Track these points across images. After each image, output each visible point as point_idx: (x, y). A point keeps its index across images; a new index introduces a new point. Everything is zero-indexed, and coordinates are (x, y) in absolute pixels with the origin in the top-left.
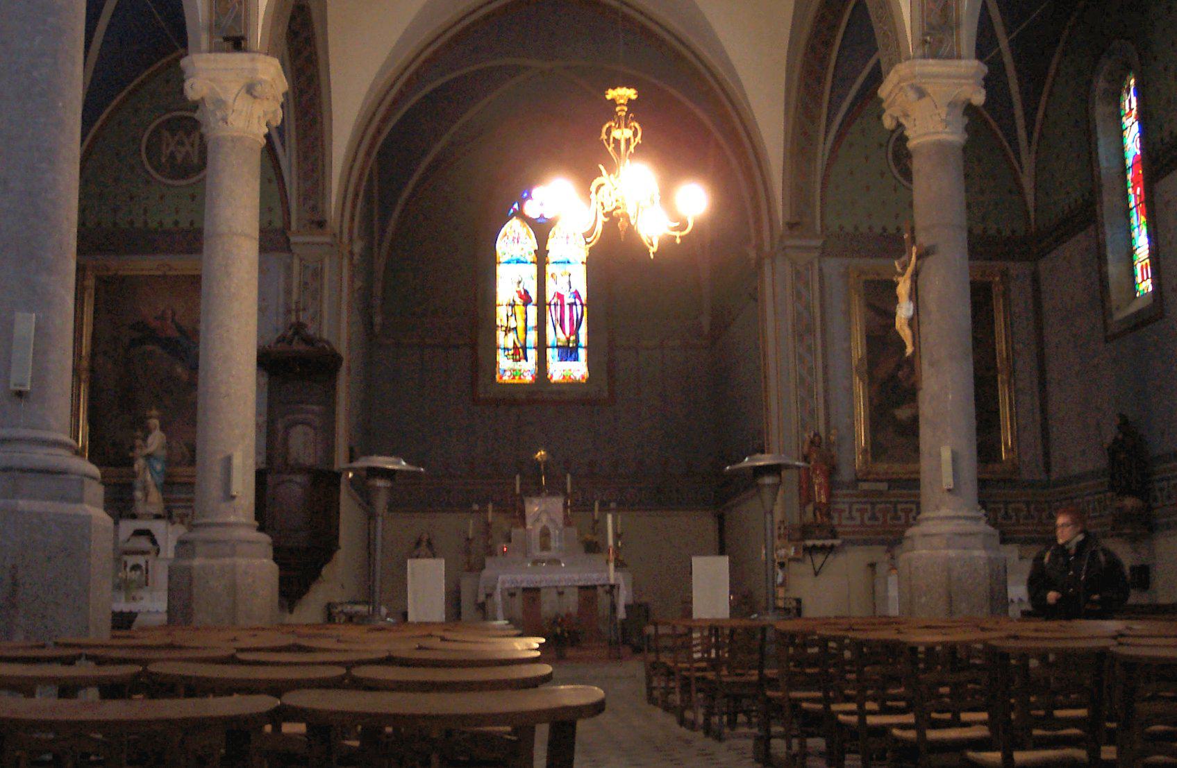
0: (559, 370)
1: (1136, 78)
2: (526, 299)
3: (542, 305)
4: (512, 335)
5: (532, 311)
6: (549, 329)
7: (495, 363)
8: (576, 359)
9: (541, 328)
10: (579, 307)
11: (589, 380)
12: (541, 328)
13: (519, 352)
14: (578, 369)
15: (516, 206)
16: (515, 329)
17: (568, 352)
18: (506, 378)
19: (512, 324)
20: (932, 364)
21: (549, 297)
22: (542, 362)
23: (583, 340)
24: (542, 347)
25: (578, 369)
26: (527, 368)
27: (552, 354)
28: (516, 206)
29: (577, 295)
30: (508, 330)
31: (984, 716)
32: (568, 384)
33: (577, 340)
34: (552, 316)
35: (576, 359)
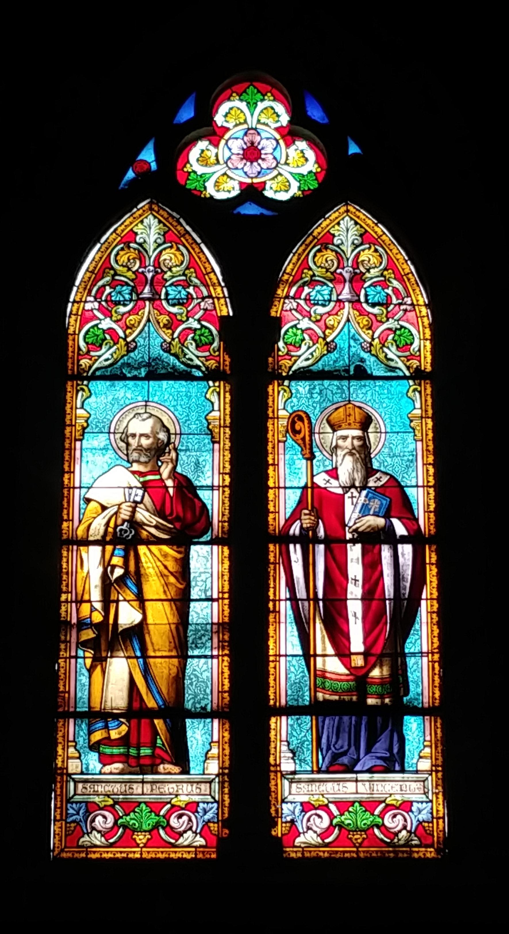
0: (314, 802)
1: (440, 719)
2: (184, 521)
3: (251, 541)
4: (119, 669)
5: (208, 564)
6: (285, 639)
7: (48, 774)
8: (394, 762)
9: (245, 634)
10: (406, 551)
11: (448, 842)
12: (245, 634)
13: (153, 730)
14: (409, 794)
15: (148, 155)
16: (139, 631)
17: (358, 723)
18: (97, 838)
19: (128, 615)
20: (124, 680)
21: (284, 502)
22: (249, 773)
23: (422, 677)
24: (248, 710)
25: (409, 794)
26: (192, 791)
27: (289, 738)
28: (148, 155)
29: (394, 496)
30: (109, 640)
31: (311, 546)
32: (369, 862)
33: (398, 681)
34: (296, 572)
35: (394, 762)
